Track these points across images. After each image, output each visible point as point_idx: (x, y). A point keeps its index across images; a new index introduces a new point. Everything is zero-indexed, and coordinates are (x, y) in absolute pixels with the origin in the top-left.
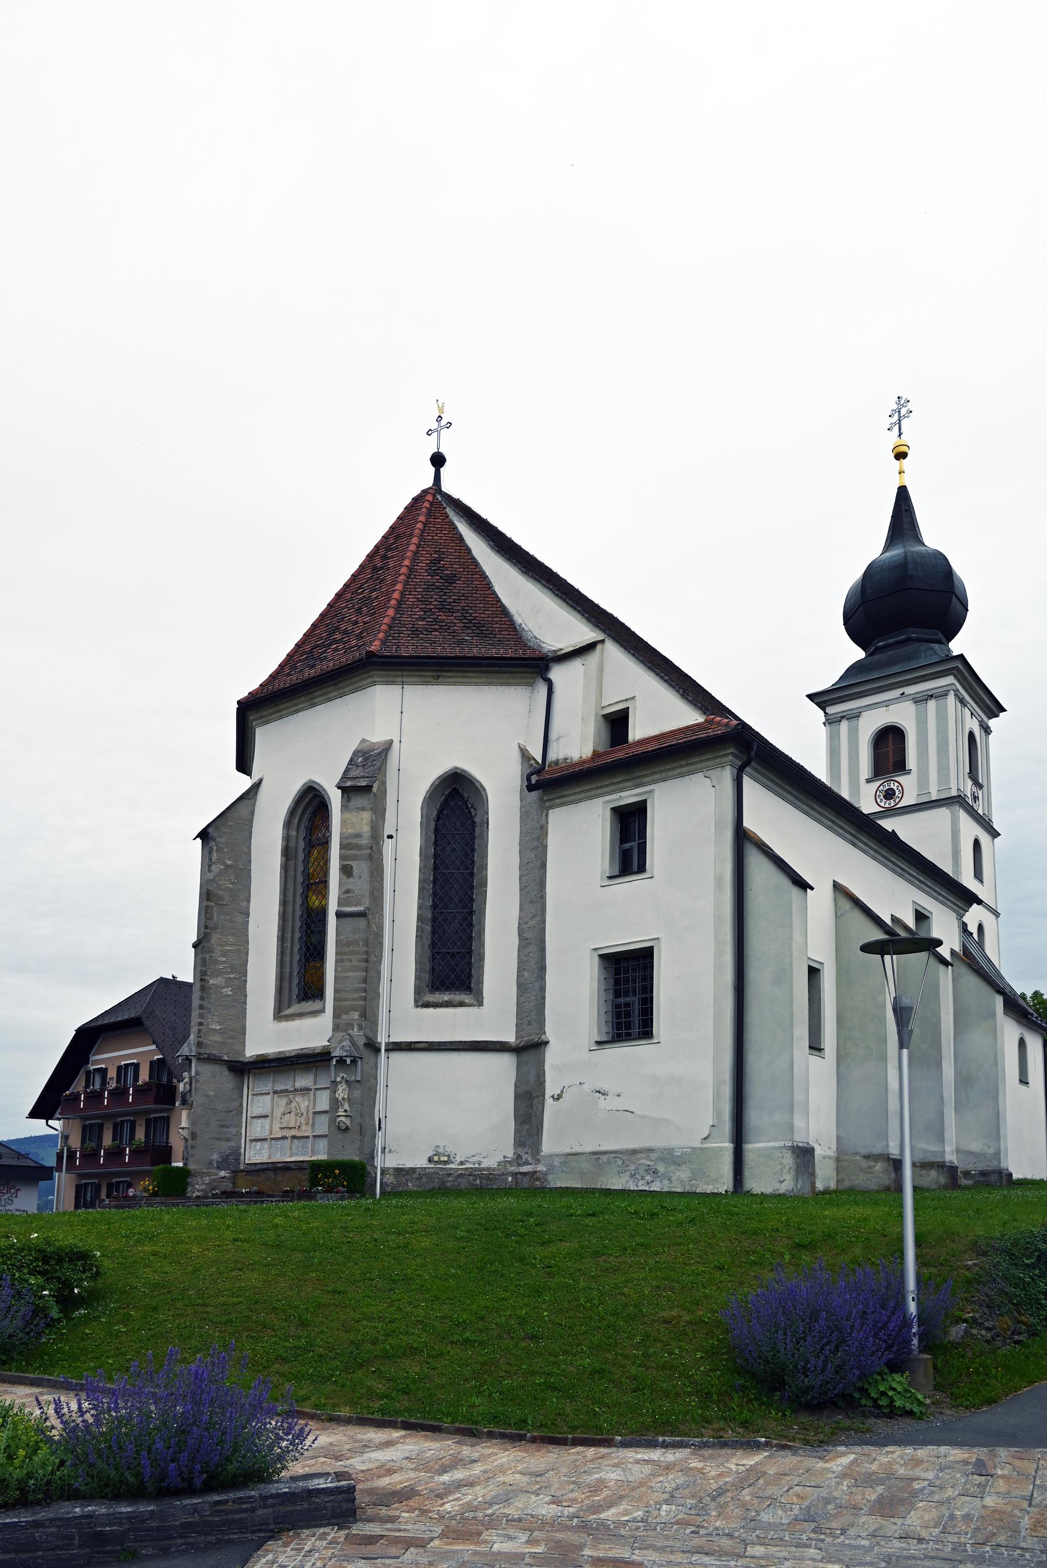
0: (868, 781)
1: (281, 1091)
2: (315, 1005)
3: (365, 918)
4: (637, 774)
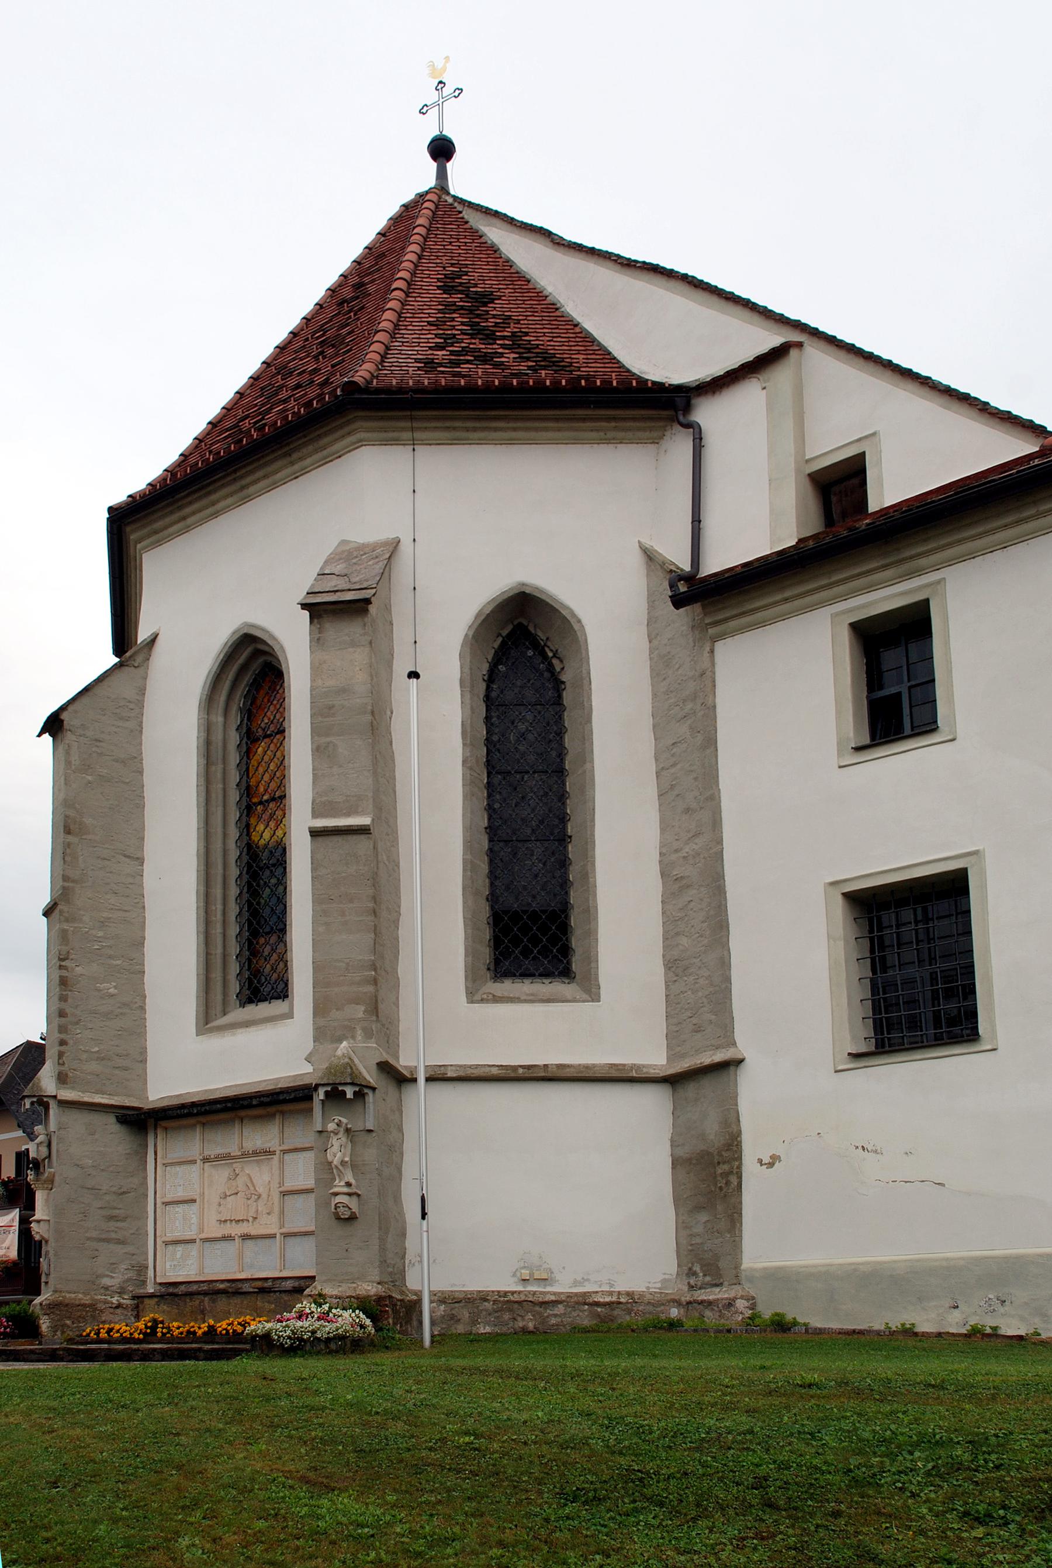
1: (219, 1158)
2: (277, 1007)
3: (361, 841)
4: (907, 553)
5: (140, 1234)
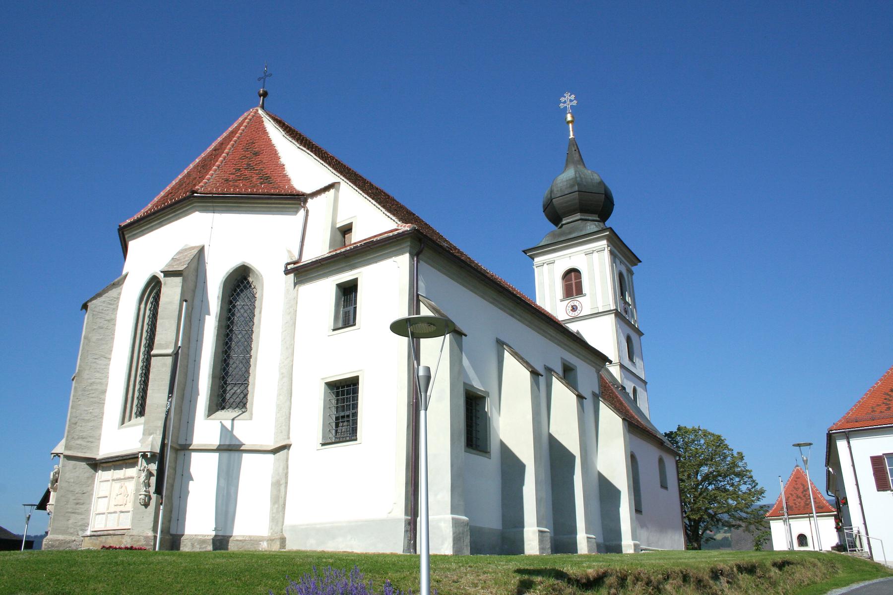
0: (561, 301)
5: (88, 511)
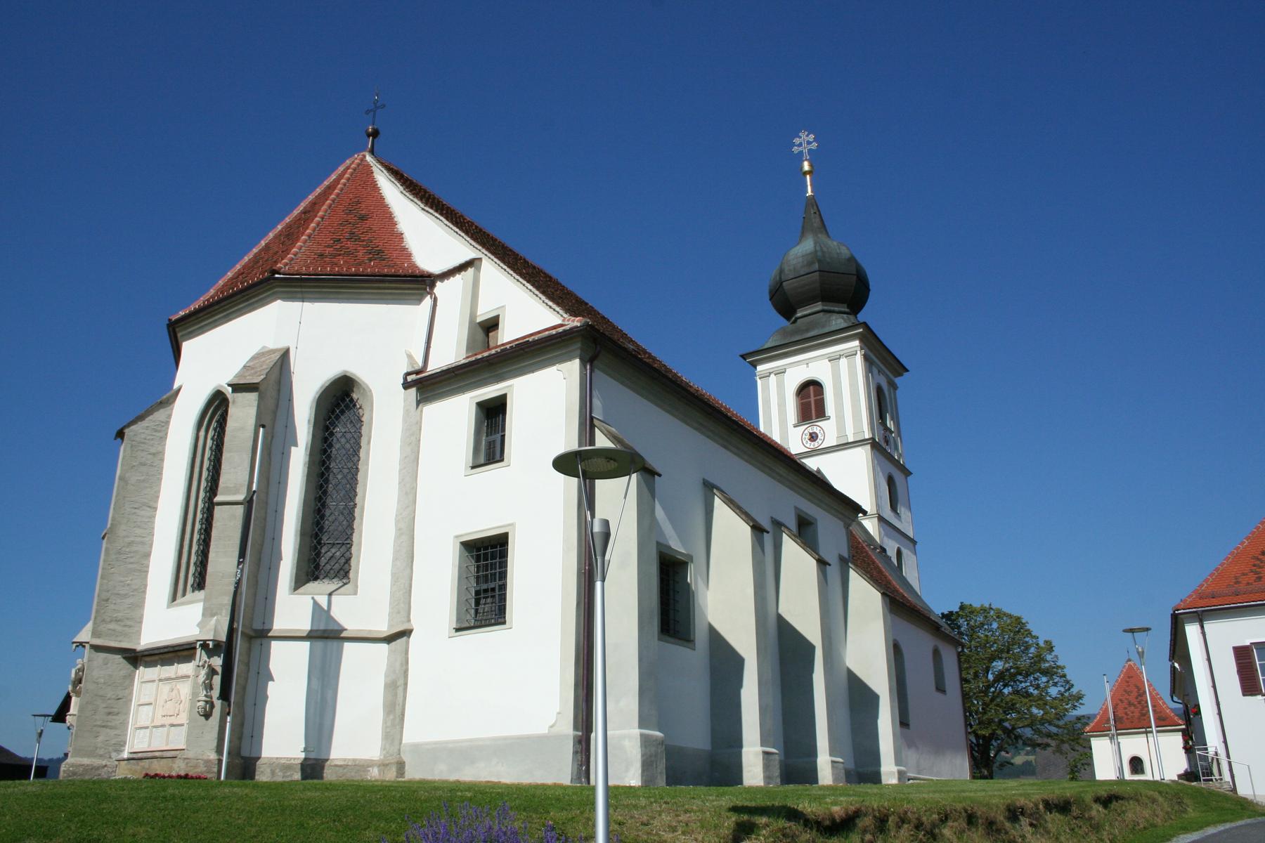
0: (795, 426)
